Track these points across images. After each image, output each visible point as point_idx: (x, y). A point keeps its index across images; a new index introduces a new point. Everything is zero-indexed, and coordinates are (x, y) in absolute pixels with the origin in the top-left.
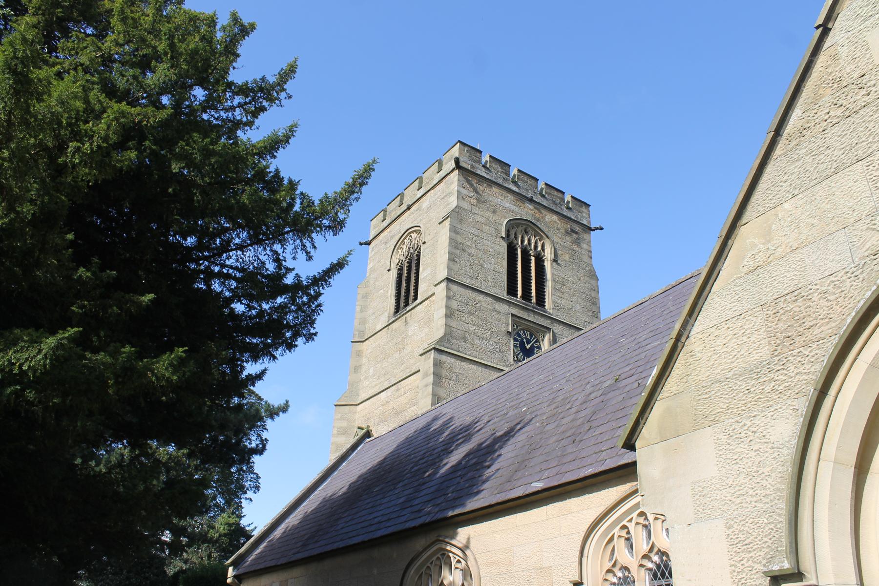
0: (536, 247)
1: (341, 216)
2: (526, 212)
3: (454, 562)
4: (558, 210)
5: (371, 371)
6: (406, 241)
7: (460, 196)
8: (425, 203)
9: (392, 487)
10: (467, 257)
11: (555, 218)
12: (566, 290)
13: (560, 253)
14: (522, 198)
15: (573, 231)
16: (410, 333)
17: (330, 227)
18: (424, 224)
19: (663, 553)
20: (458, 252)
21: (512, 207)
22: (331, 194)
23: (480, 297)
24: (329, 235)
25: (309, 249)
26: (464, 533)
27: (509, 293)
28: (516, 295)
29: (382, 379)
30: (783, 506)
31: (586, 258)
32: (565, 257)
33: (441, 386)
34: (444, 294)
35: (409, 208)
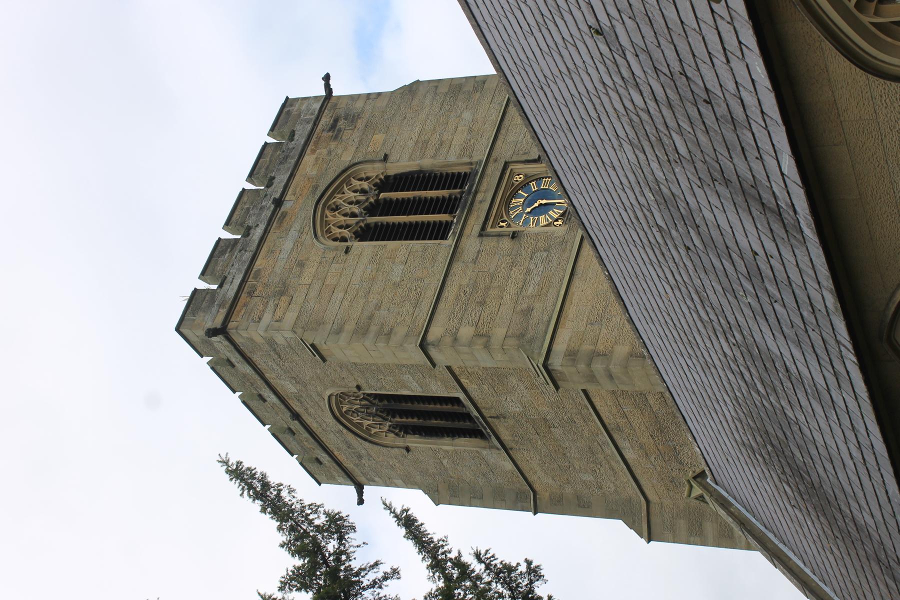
1: (320, 520)
4: (296, 153)
5: (588, 477)
6: (356, 419)
8: (288, 388)
9: (795, 428)
10: (383, 312)
11: (308, 159)
12: (436, 136)
15: (333, 127)
16: (518, 409)
17: (341, 538)
18: (326, 388)
20: (373, 329)
21: (293, 233)
22: (283, 538)
24: (353, 539)
25: (380, 575)
27: (444, 237)
28: (448, 226)
29: (600, 456)
33: (611, 352)
35: (296, 416)
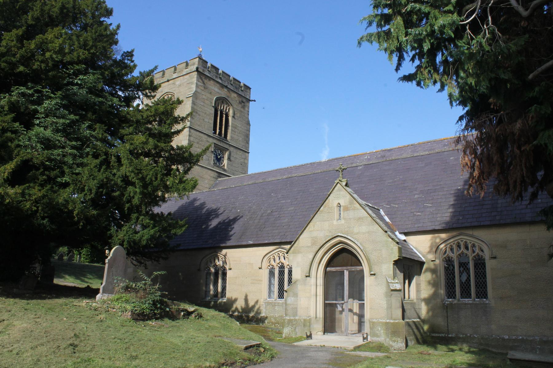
0: (226, 110)
2: (223, 93)
3: (220, 259)
7: (197, 86)
11: (235, 95)
13: (236, 113)
14: (223, 86)
15: (243, 102)
19: (282, 263)
23: (202, 135)
26: (224, 251)
30: (309, 267)
31: (246, 115)
32: (238, 115)
34: (188, 133)
35: (168, 81)
